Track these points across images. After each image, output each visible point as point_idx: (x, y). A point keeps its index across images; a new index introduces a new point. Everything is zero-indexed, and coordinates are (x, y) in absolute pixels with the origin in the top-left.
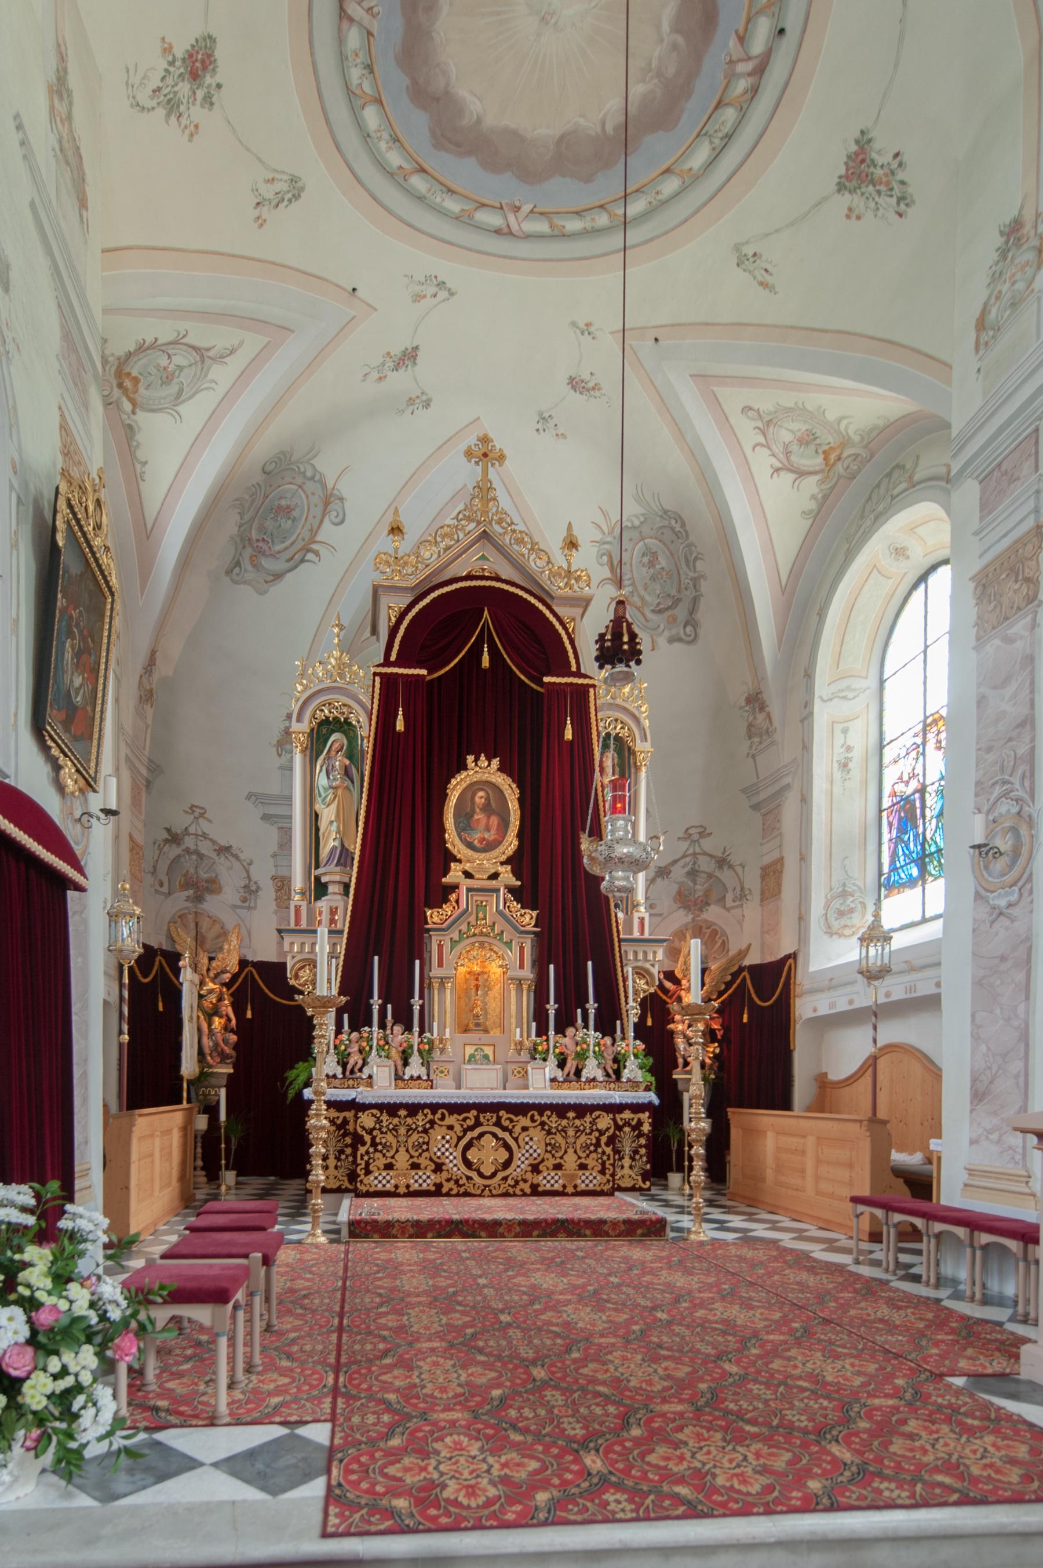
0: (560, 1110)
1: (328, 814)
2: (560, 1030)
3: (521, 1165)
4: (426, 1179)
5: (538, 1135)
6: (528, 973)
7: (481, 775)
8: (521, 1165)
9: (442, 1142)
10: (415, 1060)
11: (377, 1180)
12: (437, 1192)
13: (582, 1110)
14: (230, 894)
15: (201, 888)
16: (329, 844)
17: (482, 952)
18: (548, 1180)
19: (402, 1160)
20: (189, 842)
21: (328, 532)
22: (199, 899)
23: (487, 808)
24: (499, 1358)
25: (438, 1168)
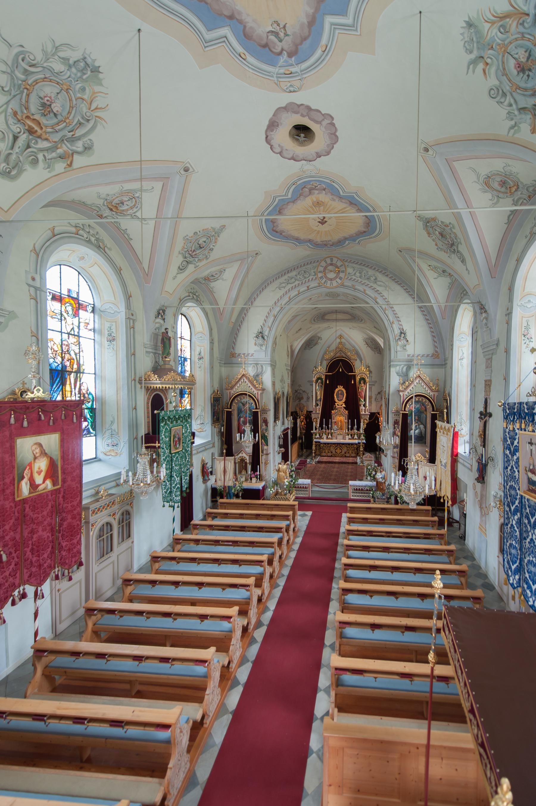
0: (349, 444)
1: (318, 393)
2: (351, 430)
3: (343, 452)
4: (330, 454)
5: (346, 448)
6: (346, 421)
7: (340, 388)
8: (343, 452)
9: (332, 449)
10: (330, 435)
11: (324, 454)
12: (331, 456)
13: (352, 444)
14: (305, 399)
15: (300, 399)
16: (319, 398)
17: (340, 417)
18: (347, 455)
19: (327, 451)
20: (298, 391)
21: (319, 341)
22: (300, 401)
23: (341, 394)
24: (40, 566)
25: (332, 453)
